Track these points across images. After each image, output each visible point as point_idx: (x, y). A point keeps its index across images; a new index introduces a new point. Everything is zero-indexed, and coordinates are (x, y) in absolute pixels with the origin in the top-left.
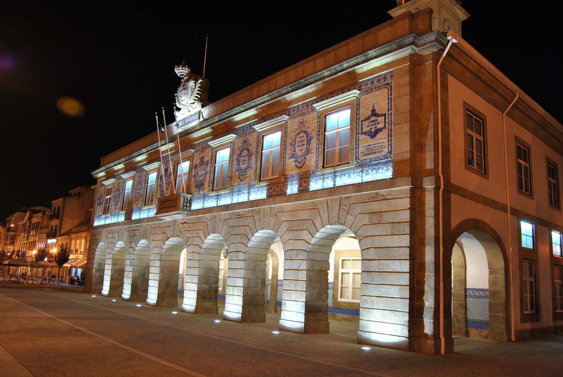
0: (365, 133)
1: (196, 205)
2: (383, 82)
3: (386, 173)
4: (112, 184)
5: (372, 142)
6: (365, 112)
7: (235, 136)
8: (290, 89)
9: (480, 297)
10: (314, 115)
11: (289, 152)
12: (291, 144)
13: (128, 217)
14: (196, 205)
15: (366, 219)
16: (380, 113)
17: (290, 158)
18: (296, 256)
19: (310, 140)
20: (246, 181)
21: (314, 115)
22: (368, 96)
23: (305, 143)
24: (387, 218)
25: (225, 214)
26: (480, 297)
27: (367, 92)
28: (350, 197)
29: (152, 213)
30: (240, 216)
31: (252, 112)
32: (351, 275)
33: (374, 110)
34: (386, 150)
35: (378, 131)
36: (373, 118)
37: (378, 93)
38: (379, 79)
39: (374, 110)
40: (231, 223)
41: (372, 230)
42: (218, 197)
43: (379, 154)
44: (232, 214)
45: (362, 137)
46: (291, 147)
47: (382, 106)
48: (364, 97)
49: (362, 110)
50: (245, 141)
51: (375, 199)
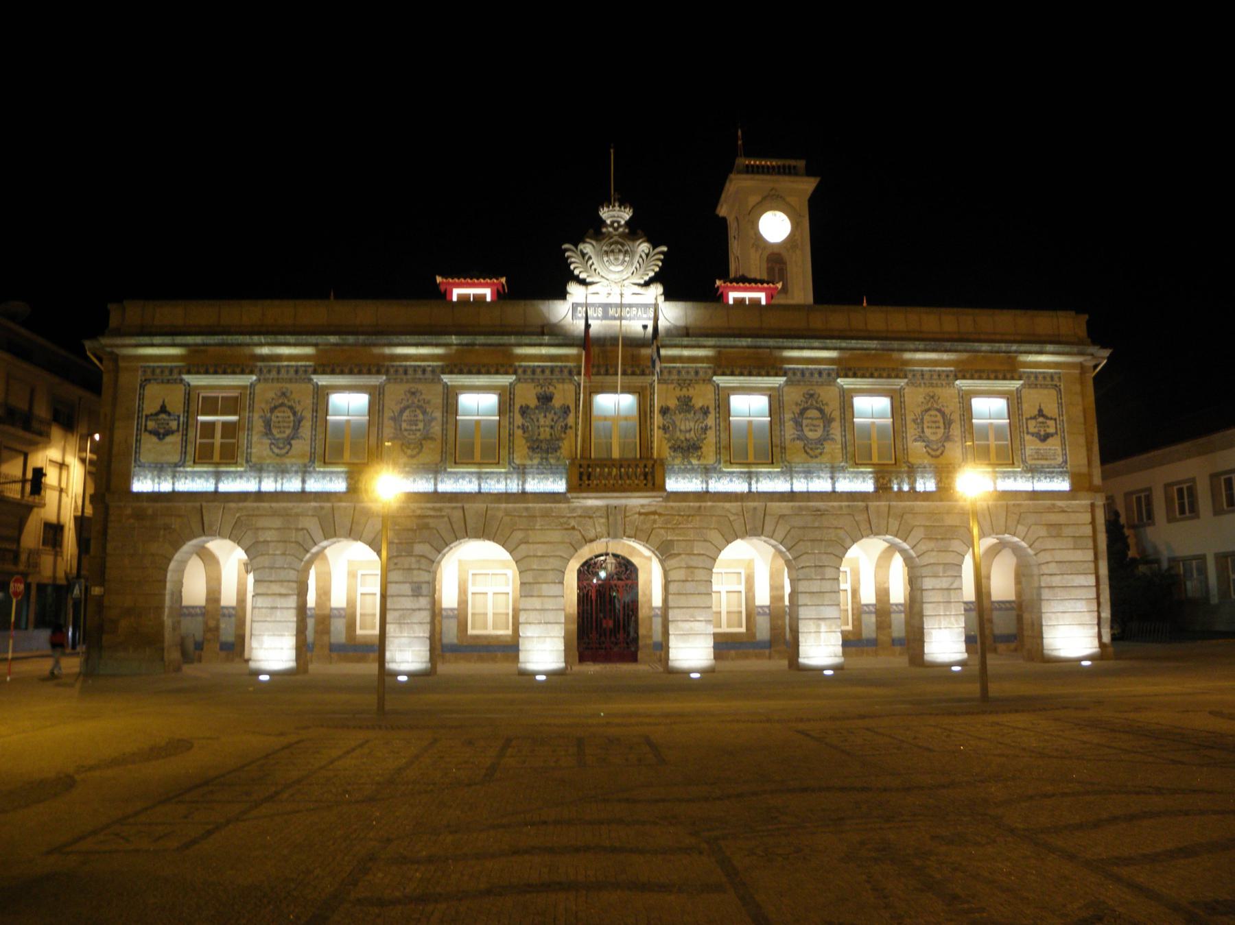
0: (1033, 435)
1: (674, 484)
2: (1048, 382)
3: (1063, 485)
4: (244, 387)
5: (1042, 446)
6: (1029, 409)
7: (785, 379)
8: (921, 347)
9: (1007, 609)
10: (954, 391)
11: (912, 431)
12: (914, 421)
13: (882, 487)
14: (674, 484)
15: (1043, 532)
16: (1049, 415)
17: (916, 440)
18: (944, 572)
19: (300, 422)
20: (825, 458)
21: (954, 391)
22: (1033, 391)
23: (942, 425)
24: (1068, 531)
25: (785, 507)
26: (1007, 609)
27: (266, 380)
28: (1019, 505)
29: (560, 486)
30: (819, 513)
31: (833, 354)
32: (490, 596)
33: (1040, 411)
34: (1060, 460)
35: (169, 432)
36: (1041, 419)
37: (1045, 391)
38: (1045, 376)
39: (1040, 411)
40: (798, 522)
41: (1049, 544)
42: (218, 476)
43: (1052, 462)
44: (800, 508)
45: (1028, 437)
46: (392, 423)
47: (1051, 409)
48: (519, 385)
49: (1025, 406)
50: (812, 396)
51: (1051, 510)
